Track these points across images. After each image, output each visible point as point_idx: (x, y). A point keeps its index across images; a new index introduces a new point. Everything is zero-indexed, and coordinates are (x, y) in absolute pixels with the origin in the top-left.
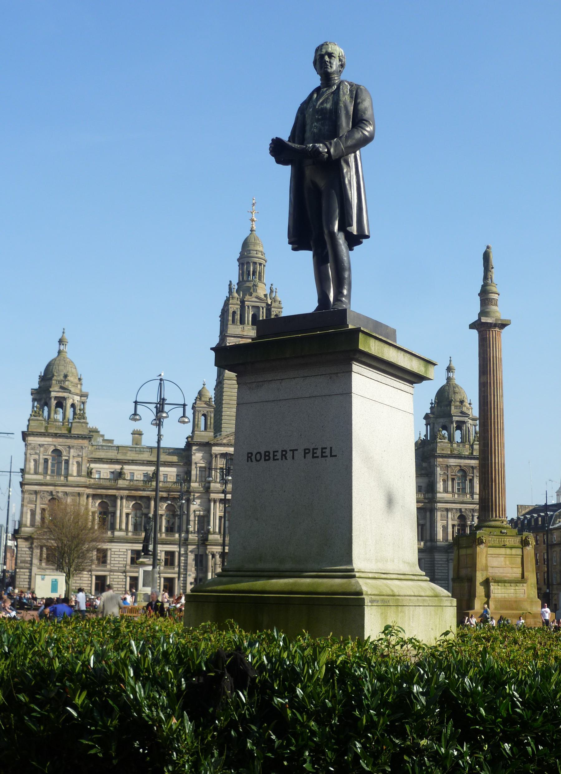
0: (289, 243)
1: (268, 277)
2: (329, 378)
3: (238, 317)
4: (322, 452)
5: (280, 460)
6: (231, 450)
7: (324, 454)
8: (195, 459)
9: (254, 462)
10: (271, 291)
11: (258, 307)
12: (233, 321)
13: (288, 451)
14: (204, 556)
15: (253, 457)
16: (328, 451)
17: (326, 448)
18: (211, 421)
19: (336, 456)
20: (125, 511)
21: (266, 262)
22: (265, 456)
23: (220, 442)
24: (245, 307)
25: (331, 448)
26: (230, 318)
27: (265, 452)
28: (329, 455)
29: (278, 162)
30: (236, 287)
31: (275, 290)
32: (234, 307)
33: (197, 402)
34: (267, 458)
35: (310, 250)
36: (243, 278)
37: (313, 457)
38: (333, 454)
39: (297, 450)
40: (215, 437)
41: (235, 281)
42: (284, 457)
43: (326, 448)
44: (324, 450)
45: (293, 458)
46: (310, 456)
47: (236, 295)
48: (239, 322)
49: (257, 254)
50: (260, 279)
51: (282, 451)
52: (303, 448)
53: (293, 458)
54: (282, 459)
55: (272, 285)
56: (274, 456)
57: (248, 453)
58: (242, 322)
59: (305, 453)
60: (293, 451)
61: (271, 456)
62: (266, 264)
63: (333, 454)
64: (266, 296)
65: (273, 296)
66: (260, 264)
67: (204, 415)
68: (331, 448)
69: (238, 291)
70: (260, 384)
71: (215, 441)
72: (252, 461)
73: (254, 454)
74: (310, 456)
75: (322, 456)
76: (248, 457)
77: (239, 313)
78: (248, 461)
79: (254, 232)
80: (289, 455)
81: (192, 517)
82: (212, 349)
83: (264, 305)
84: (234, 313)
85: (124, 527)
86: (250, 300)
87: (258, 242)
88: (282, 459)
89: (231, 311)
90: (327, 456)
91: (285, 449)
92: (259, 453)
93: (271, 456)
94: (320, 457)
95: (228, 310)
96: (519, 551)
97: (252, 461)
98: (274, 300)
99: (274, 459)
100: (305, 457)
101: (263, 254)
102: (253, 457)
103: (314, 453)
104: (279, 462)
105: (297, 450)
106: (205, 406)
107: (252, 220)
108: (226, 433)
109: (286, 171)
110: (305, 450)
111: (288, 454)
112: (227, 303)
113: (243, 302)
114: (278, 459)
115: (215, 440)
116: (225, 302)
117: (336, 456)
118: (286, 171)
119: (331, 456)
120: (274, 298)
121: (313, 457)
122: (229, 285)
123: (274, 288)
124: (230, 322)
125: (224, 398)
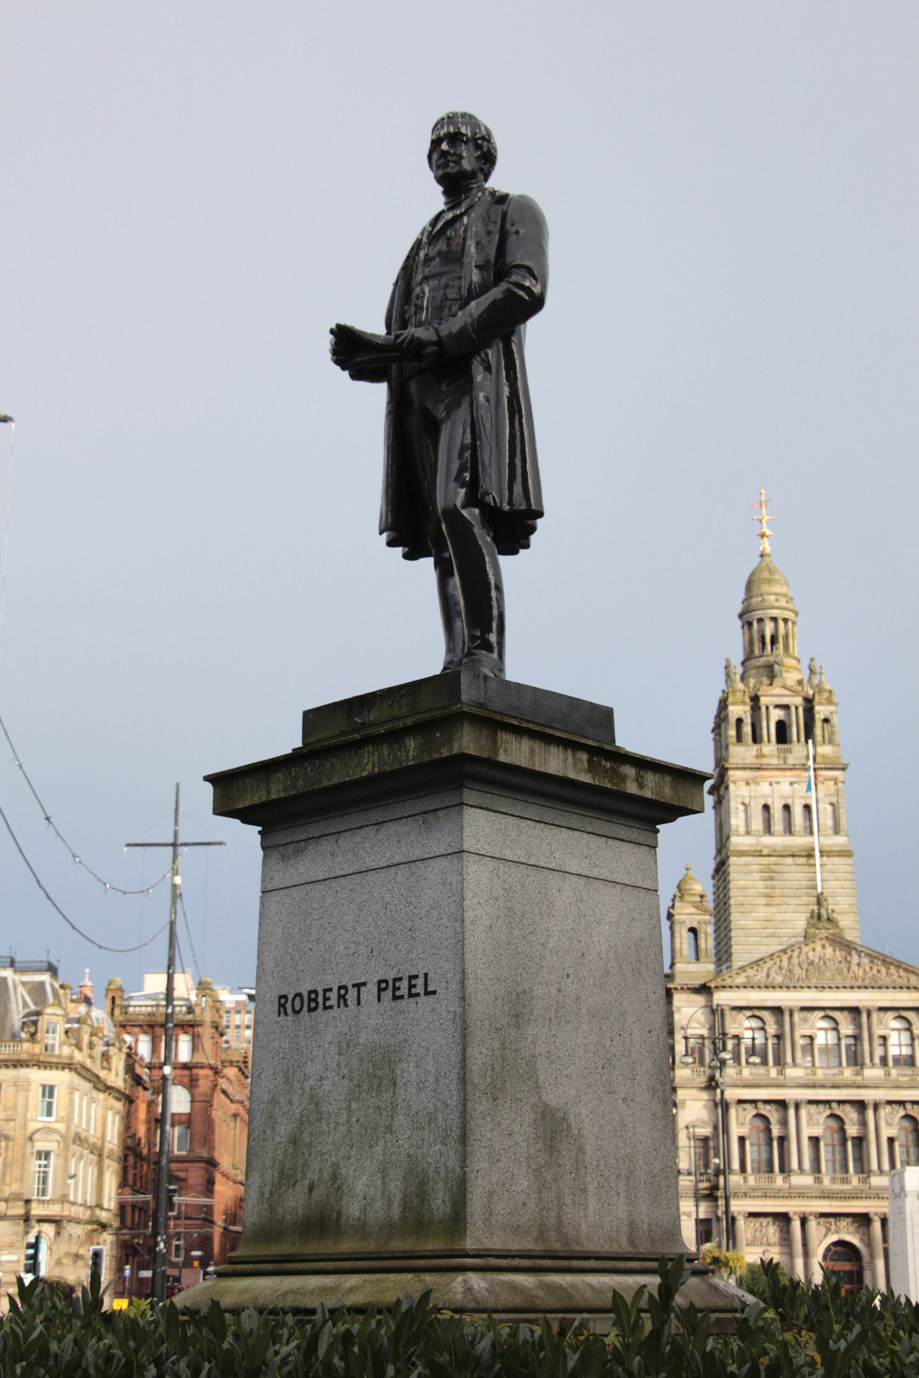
0: (391, 543)
1: (800, 645)
2: (421, 822)
3: (747, 729)
4: (411, 986)
5: (335, 1008)
6: (253, 992)
7: (413, 991)
8: (680, 1021)
9: (291, 1016)
10: (812, 671)
11: (786, 707)
12: (739, 738)
13: (350, 987)
14: (714, 1223)
15: (289, 1006)
16: (420, 982)
17: (416, 977)
18: (708, 942)
19: (434, 992)
20: (807, 1132)
21: (797, 614)
22: (310, 1000)
23: (728, 982)
24: (759, 708)
25: (426, 975)
26: (732, 732)
27: (310, 992)
28: (422, 992)
29: (356, 376)
30: (739, 670)
31: (818, 670)
32: (739, 710)
33: (677, 904)
34: (313, 1005)
35: (429, 555)
36: (752, 651)
37: (395, 998)
38: (429, 990)
39: (364, 984)
40: (719, 972)
41: (738, 657)
42: (342, 1001)
43: (416, 977)
44: (413, 982)
45: (359, 1003)
46: (387, 995)
47: (740, 686)
48: (750, 739)
49: (776, 600)
50: (786, 648)
51: (340, 988)
52: (376, 980)
53: (359, 1003)
54: (339, 1007)
55: (812, 660)
56: (326, 999)
57: (281, 997)
58: (756, 739)
59: (380, 990)
60: (358, 986)
61: (320, 999)
62: (798, 620)
63: (429, 990)
64: (800, 682)
65: (816, 681)
66: (786, 621)
67: (693, 930)
68: (426, 975)
69: (743, 679)
70: (302, 844)
71: (719, 982)
72: (286, 1014)
73: (290, 997)
74: (387, 995)
75: (411, 995)
76: (280, 1005)
77: (748, 720)
78: (279, 1015)
79: (767, 559)
80: (352, 994)
81: (683, 1139)
82: (207, 779)
83: (799, 701)
84: (739, 721)
85: (807, 1165)
86: (769, 693)
87: (777, 577)
88: (339, 1007)
89: (732, 719)
90: (418, 995)
91: (344, 983)
92: (299, 995)
93: (320, 999)
94: (406, 996)
95: (727, 717)
96: (80, 1201)
97: (286, 1014)
98: (819, 689)
99: (326, 1008)
100: (379, 1000)
101: (790, 599)
102: (289, 1006)
103: (396, 989)
104: (335, 1012)
105: (364, 984)
106: (693, 910)
107: (763, 536)
108: (740, 964)
109: (375, 396)
110: (380, 982)
111: (350, 993)
112: (723, 705)
113: (755, 699)
114: (331, 1007)
115: (719, 980)
116: (721, 701)
117: (434, 992)
118: (375, 396)
119: (427, 993)
120: (817, 686)
121: (395, 998)
122: (726, 668)
123: (816, 665)
124: (734, 740)
125: (732, 893)
